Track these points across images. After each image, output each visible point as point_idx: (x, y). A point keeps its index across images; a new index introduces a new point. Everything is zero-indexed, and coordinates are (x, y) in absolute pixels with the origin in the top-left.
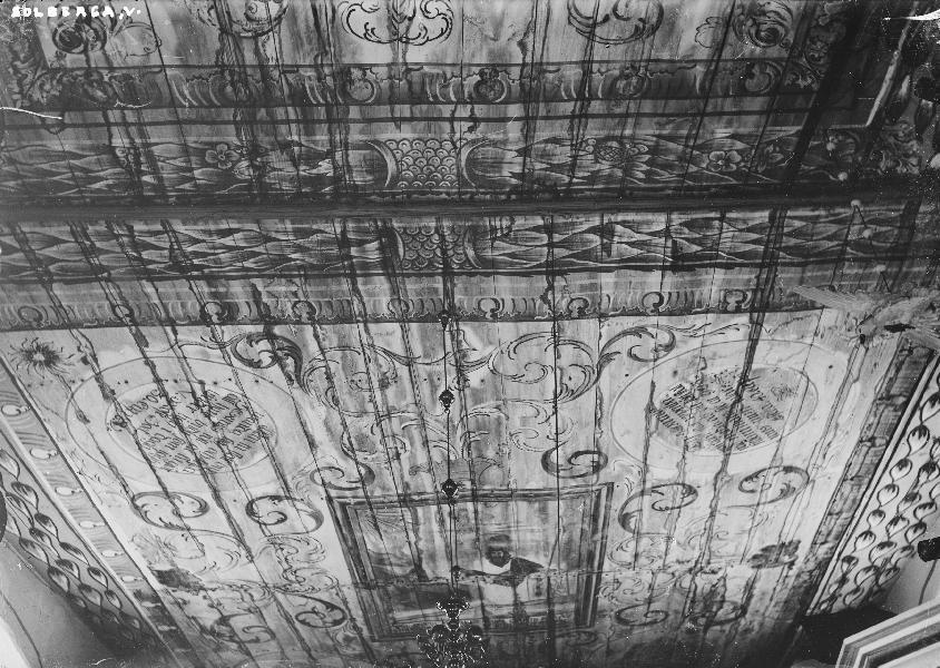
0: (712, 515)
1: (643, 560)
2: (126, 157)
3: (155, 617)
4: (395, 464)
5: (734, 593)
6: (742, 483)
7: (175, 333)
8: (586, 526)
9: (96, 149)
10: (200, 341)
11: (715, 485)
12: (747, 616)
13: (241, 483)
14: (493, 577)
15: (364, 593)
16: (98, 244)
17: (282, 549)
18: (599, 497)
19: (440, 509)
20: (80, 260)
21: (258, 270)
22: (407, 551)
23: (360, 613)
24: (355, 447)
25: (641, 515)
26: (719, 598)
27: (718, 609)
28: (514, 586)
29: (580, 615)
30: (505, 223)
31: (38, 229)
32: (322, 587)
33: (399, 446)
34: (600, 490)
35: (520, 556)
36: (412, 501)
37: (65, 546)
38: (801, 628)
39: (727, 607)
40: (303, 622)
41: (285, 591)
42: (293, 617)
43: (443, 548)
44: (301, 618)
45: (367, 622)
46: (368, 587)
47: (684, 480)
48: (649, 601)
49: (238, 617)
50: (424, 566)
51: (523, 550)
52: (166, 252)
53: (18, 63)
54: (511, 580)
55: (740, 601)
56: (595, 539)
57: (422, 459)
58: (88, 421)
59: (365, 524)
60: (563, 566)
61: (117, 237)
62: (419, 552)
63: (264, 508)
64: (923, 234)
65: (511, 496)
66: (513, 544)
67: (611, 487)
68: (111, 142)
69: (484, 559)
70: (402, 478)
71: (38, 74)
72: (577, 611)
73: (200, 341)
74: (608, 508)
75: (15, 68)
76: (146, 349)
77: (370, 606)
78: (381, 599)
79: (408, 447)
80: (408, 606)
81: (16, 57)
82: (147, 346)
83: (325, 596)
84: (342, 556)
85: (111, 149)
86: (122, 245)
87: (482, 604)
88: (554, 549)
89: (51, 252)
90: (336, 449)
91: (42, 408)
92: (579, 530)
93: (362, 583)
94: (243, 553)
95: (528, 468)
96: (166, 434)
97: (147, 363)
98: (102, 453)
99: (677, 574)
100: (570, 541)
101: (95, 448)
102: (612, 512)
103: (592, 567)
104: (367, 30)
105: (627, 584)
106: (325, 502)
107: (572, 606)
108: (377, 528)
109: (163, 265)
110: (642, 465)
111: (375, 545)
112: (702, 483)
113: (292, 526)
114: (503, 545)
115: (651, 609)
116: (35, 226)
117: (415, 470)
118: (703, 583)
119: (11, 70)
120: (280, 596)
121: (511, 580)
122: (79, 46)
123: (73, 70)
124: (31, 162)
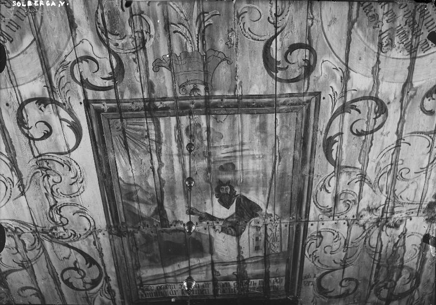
0: (398, 145)
1: (341, 207)
4: (141, 55)
5: (410, 257)
6: (423, 99)
8: (297, 153)
11: (402, 100)
12: (420, 287)
14: (221, 223)
15: (117, 241)
17: (48, 176)
18: (308, 111)
19: (178, 122)
22: (151, 181)
23: (114, 270)
24: (108, 28)
25: (341, 139)
26: (398, 263)
27: (398, 279)
28: (238, 235)
29: (290, 276)
32: (82, 232)
33: (145, 29)
34: (309, 102)
35: (244, 194)
36: (156, 108)
37: (66, 101)
39: (405, 275)
40: (67, 282)
41: (54, 238)
42: (59, 272)
43: (181, 179)
44: (66, 275)
45: (119, 284)
46: (120, 234)
47: (377, 94)
48: (344, 265)
49: (15, 273)
50: (166, 204)
51: (245, 185)
54: (234, 228)
55: (414, 267)
56: (304, 173)
57: (164, 52)
59: (117, 142)
60: (278, 210)
62: (162, 183)
63: (33, 113)
65: (236, 106)
66: (239, 175)
67: (317, 95)
69: (214, 197)
70: (148, 76)
72: (287, 272)
74: (316, 128)
77: (121, 260)
78: (131, 250)
79: (153, 33)
80: (153, 263)
83: (82, 245)
84: (98, 188)
87: (212, 261)
88: (271, 184)
90: (92, 30)
92: (291, 159)
93: (116, 228)
94: (16, 179)
95: (252, 66)
99: (367, 226)
100: (284, 174)
102: (319, 134)
103: (300, 213)
104: (313, 254)
105: (328, 238)
106: (82, 107)
107: (283, 268)
108: (126, 147)
110: (344, 68)
111: (125, 172)
112: (392, 98)
113: (56, 144)
114: (229, 177)
115: (346, 276)
117: (158, 65)
118: (388, 237)
120: (47, 244)
121: (234, 228)
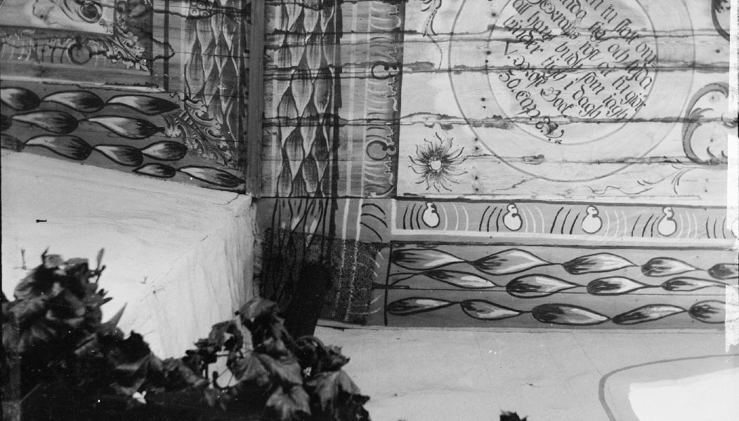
2: (200, 10)
3: (227, 82)
7: (412, 32)
9: (190, 30)
10: (428, 14)
13: (680, 33)
16: (295, 63)
20: (313, 85)
21: (323, 213)
30: (351, 296)
31: (275, 105)
38: (49, 365)
52: (307, 11)
53: (109, 54)
58: (541, 157)
61: (286, 46)
64: (329, 194)
68: (185, 16)
71: (118, 43)
73: (428, 14)
75: (111, 57)
76: (436, 67)
81: (104, 53)
82: (432, 65)
85: (190, 18)
86: (296, 45)
89: (301, 105)
91: (509, 192)
96: (576, 87)
97: (458, 72)
98: (599, 162)
101: (588, 166)
107: (296, 122)
109: (323, 20)
116: (271, 106)
119: (114, 61)
122: (96, 8)
123: (115, 19)
124: (201, 81)
